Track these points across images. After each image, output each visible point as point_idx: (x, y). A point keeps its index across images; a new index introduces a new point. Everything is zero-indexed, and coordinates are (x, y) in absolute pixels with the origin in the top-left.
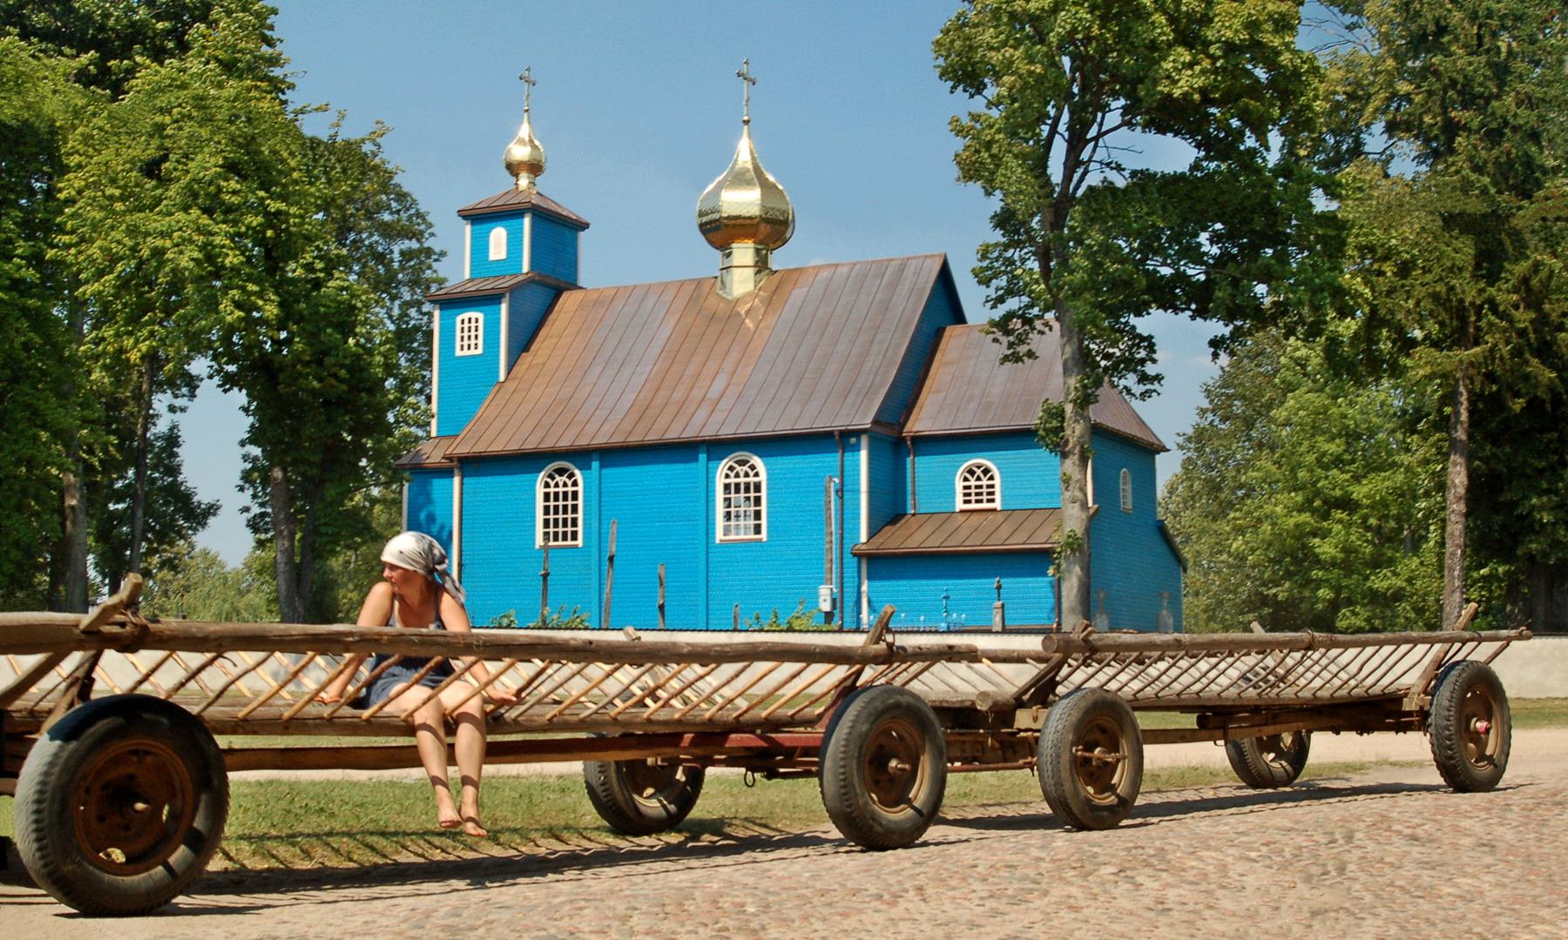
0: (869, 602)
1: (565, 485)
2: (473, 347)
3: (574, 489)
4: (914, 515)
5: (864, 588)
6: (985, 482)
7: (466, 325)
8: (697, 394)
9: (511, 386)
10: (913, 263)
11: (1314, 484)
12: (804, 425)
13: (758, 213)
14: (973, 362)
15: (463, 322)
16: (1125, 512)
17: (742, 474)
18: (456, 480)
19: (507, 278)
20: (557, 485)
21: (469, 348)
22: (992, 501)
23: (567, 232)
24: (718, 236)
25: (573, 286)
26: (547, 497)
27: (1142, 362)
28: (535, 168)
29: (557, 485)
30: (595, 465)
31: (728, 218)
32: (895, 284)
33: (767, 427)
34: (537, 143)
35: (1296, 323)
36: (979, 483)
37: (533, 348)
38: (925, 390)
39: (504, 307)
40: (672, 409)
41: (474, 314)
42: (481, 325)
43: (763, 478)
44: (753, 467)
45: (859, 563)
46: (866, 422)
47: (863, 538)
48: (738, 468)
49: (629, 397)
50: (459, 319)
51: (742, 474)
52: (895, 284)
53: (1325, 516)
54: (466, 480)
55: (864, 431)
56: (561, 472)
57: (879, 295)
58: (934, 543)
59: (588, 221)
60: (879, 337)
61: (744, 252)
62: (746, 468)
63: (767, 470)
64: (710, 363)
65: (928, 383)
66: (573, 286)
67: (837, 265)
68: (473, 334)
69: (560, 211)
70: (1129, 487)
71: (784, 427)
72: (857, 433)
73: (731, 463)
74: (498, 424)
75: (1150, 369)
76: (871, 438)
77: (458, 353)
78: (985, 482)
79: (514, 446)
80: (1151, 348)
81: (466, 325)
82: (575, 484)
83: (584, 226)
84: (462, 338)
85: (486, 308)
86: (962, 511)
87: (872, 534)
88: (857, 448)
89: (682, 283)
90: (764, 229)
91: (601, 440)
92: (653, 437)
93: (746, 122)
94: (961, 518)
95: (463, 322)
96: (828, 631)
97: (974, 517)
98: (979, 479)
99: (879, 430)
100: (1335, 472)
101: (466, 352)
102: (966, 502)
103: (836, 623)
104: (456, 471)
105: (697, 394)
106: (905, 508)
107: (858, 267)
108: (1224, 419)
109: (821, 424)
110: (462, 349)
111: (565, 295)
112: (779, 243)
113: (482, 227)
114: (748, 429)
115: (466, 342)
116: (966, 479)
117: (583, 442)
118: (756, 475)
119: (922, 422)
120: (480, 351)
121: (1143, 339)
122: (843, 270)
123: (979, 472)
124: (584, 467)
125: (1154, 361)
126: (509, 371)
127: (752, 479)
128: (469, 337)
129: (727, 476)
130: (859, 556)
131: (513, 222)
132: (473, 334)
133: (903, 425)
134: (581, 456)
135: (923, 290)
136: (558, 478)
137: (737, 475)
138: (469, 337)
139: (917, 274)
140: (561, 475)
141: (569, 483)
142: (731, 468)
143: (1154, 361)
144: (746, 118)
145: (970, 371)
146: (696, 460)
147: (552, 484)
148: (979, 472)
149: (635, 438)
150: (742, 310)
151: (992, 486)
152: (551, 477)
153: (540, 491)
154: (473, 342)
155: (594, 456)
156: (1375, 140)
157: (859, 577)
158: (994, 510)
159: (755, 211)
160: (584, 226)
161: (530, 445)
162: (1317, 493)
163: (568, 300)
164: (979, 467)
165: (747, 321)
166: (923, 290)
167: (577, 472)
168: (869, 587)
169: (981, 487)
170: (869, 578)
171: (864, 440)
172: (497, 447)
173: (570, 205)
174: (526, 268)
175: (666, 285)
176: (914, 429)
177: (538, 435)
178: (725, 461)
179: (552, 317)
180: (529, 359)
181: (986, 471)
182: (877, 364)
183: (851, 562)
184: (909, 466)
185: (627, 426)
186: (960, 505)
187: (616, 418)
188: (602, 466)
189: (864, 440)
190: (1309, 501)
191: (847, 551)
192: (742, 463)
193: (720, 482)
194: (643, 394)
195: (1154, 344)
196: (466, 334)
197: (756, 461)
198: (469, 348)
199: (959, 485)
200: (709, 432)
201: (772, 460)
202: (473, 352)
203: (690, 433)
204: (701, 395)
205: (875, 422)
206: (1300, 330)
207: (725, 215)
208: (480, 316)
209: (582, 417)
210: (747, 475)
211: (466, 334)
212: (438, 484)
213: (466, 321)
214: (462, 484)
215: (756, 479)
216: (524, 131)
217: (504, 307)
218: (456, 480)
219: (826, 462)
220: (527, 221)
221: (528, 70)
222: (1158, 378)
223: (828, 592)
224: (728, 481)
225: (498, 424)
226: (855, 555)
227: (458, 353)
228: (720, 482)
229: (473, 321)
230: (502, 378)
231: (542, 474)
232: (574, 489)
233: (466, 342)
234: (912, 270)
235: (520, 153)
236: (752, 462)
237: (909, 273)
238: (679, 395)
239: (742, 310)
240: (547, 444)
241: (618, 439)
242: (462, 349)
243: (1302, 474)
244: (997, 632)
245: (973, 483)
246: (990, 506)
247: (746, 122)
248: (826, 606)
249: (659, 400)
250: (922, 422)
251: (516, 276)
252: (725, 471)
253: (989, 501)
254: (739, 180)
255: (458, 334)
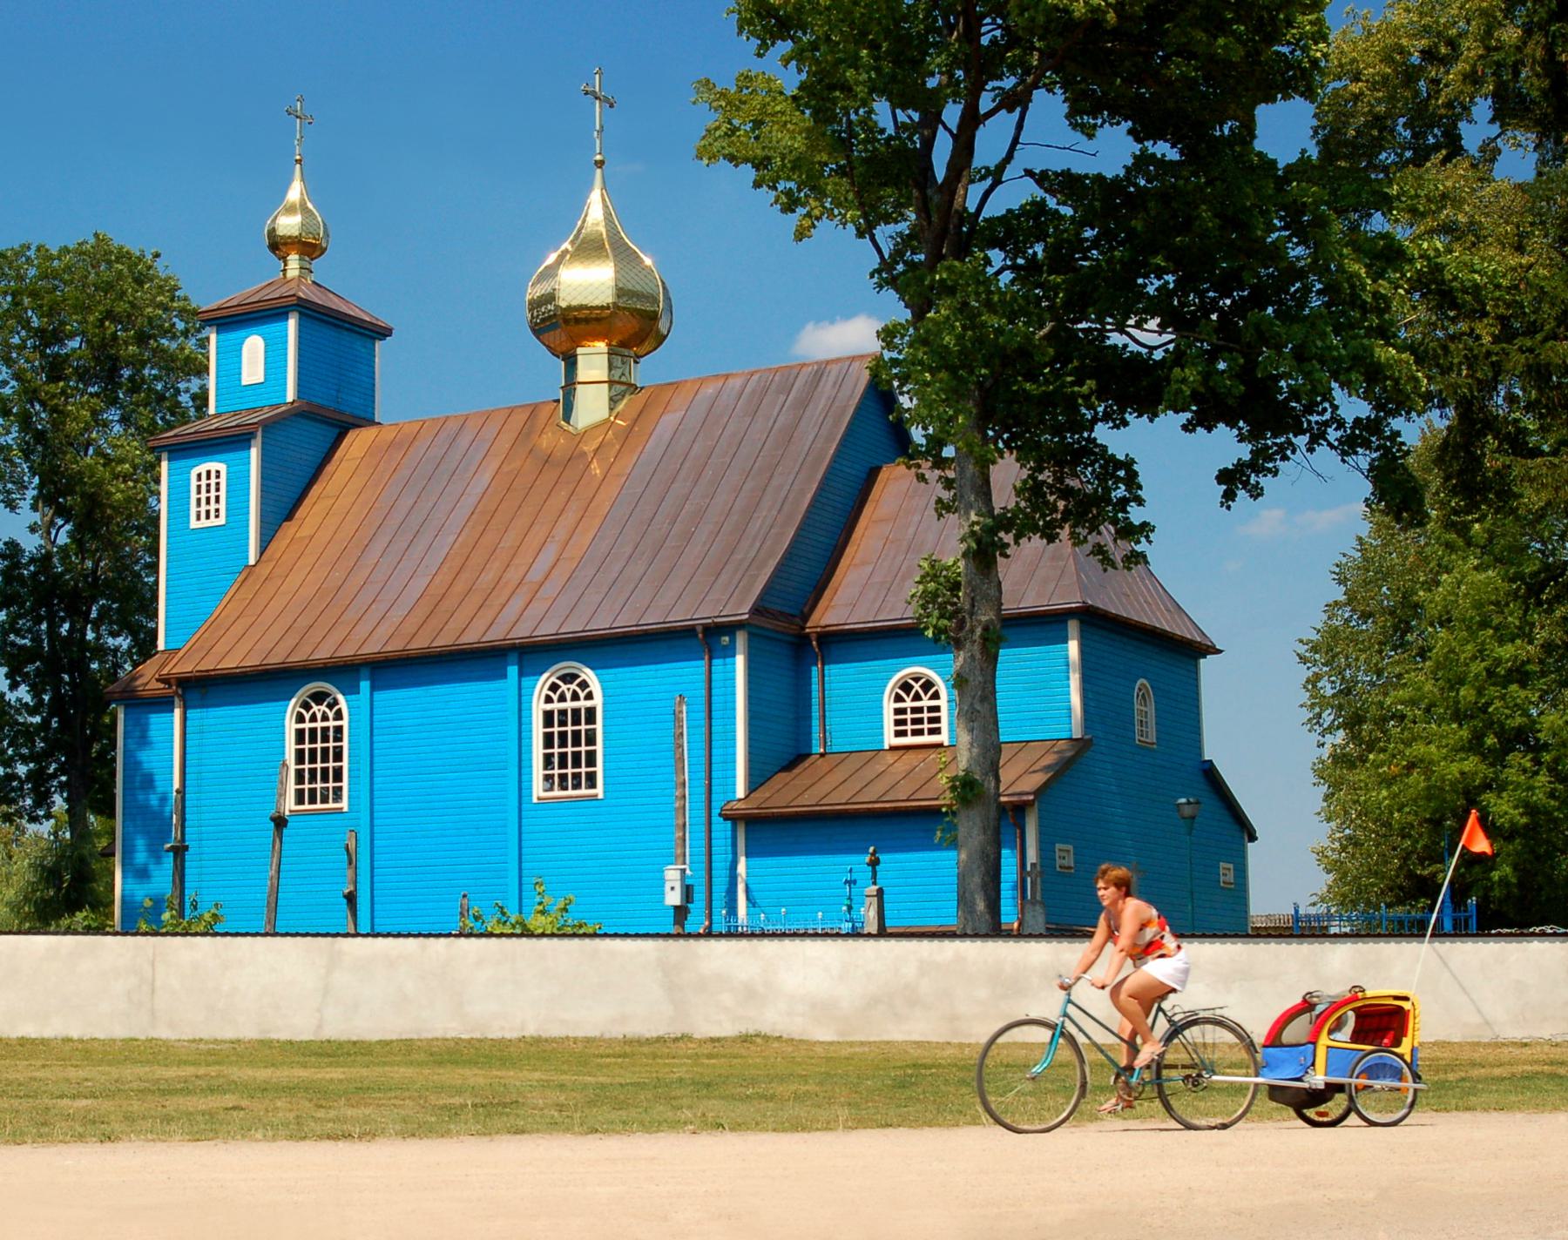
0: (747, 890)
1: (325, 718)
2: (212, 514)
3: (338, 723)
4: (822, 755)
5: (741, 868)
6: (926, 702)
7: (204, 482)
8: (513, 575)
9: (264, 570)
10: (835, 368)
11: (1484, 709)
12: (652, 619)
13: (610, 300)
14: (916, 518)
15: (199, 476)
16: (1144, 748)
17: (568, 696)
18: (177, 712)
19: (265, 410)
20: (313, 719)
21: (208, 517)
22: (936, 731)
23: (359, 344)
24: (558, 337)
25: (370, 422)
26: (300, 734)
27: (1123, 504)
28: (310, 249)
29: (313, 719)
30: (365, 685)
31: (569, 308)
32: (804, 403)
33: (602, 623)
34: (310, 205)
35: (1326, 424)
36: (917, 704)
37: (298, 515)
38: (844, 562)
39: (254, 453)
40: (475, 599)
41: (213, 466)
42: (223, 480)
43: (598, 702)
44: (583, 685)
45: (734, 831)
46: (743, 611)
47: (740, 792)
48: (564, 687)
49: (419, 584)
50: (194, 473)
51: (568, 696)
52: (804, 403)
53: (1497, 758)
54: (191, 713)
55: (740, 625)
56: (319, 697)
57: (781, 419)
58: (840, 798)
59: (391, 324)
60: (774, 482)
61: (593, 360)
62: (573, 686)
63: (603, 689)
64: (536, 527)
65: (849, 551)
66: (370, 422)
67: (727, 377)
68: (213, 494)
69: (344, 308)
70: (1151, 709)
71: (626, 621)
72: (730, 628)
73: (553, 679)
74: (238, 629)
75: (1136, 515)
76: (752, 637)
77: (194, 524)
78: (926, 702)
79: (253, 661)
80: (1132, 480)
81: (204, 482)
82: (339, 716)
83: (385, 333)
84: (199, 500)
85: (231, 456)
86: (893, 748)
87: (753, 786)
88: (730, 652)
89: (512, 410)
90: (628, 325)
91: (372, 648)
92: (444, 641)
93: (600, 164)
94: (890, 757)
95: (199, 476)
96: (501, 935)
97: (910, 757)
98: (917, 698)
99: (761, 621)
100: (1514, 687)
101: (204, 523)
102: (899, 734)
103: (696, 922)
104: (177, 700)
105: (513, 575)
106: (810, 746)
107: (755, 377)
108: (1365, 616)
109: (679, 616)
110: (198, 518)
111: (351, 435)
112: (646, 346)
113: (233, 336)
114: (575, 626)
115: (204, 508)
116: (898, 699)
117: (347, 651)
118: (589, 696)
119: (834, 612)
120: (222, 521)
121: (1119, 465)
122: (735, 383)
123: (917, 687)
124: (350, 690)
125: (1140, 502)
126: (263, 550)
127: (583, 704)
128: (208, 501)
129: (549, 700)
130: (732, 818)
131: (273, 328)
132: (213, 494)
133: (806, 618)
134: (345, 672)
135: (845, 408)
136: (315, 708)
137: (562, 699)
138: (208, 501)
139: (839, 385)
140: (319, 703)
141: (331, 715)
142: (554, 687)
143: (1140, 502)
144: (598, 157)
145: (911, 530)
146: (504, 676)
147: (307, 716)
148: (917, 687)
149: (420, 643)
150: (589, 448)
151: (937, 709)
152: (307, 706)
153: (291, 727)
154: (213, 506)
155: (365, 672)
156: (1476, 130)
157: (735, 854)
158: (940, 745)
159: (605, 297)
160: (385, 333)
161: (275, 659)
162: (1489, 725)
163: (357, 443)
164: (917, 680)
165: (594, 465)
166: (845, 408)
167: (340, 697)
168: (747, 868)
169: (920, 710)
170: (747, 856)
171: (741, 640)
172: (230, 663)
173: (361, 302)
174: (290, 397)
175: (488, 415)
176: (823, 623)
177: (290, 642)
178: (545, 675)
179: (329, 468)
180: (292, 531)
181: (928, 685)
182: (769, 522)
183: (722, 829)
184: (815, 680)
185: (409, 627)
186: (890, 740)
187: (397, 615)
188: (373, 688)
189: (741, 640)
190: (1478, 737)
191: (715, 812)
192: (569, 678)
193: (538, 708)
194: (437, 580)
195: (1136, 474)
196: (204, 495)
197: (588, 674)
198: (208, 517)
199: (889, 706)
200: (522, 632)
201: (611, 673)
202: (213, 522)
203: (496, 635)
204: (518, 577)
205: (757, 610)
206: (1333, 434)
207: (563, 304)
208: (222, 468)
209: (351, 615)
210: (575, 697)
211: (204, 495)
212: (156, 720)
213: (204, 476)
214: (184, 720)
215: (589, 704)
216: (295, 193)
217: (254, 453)
218: (177, 712)
219: (686, 674)
220: (292, 324)
221: (301, 100)
222: (1145, 528)
223: (677, 875)
224: (549, 707)
225: (238, 629)
226: (726, 818)
227: (194, 524)
228: (538, 708)
229: (213, 475)
230: (252, 561)
231: (294, 700)
232: (338, 723)
233: (204, 508)
234: (832, 379)
235: (289, 224)
236: (583, 677)
237: (827, 387)
238: (488, 577)
239: (589, 448)
240: (298, 657)
241: (395, 646)
242: (198, 518)
243: (1466, 693)
244: (869, 935)
245: (909, 703)
246: (934, 739)
247: (600, 164)
248: (674, 898)
249: (459, 587)
250: (834, 612)
251: (278, 406)
252: (545, 691)
253: (933, 732)
254: (589, 249)
255: (194, 496)
